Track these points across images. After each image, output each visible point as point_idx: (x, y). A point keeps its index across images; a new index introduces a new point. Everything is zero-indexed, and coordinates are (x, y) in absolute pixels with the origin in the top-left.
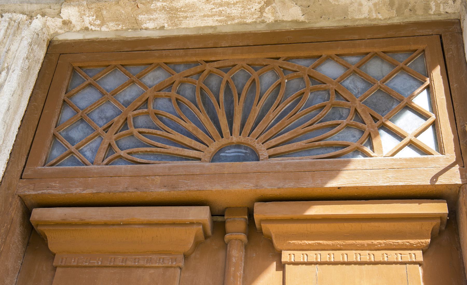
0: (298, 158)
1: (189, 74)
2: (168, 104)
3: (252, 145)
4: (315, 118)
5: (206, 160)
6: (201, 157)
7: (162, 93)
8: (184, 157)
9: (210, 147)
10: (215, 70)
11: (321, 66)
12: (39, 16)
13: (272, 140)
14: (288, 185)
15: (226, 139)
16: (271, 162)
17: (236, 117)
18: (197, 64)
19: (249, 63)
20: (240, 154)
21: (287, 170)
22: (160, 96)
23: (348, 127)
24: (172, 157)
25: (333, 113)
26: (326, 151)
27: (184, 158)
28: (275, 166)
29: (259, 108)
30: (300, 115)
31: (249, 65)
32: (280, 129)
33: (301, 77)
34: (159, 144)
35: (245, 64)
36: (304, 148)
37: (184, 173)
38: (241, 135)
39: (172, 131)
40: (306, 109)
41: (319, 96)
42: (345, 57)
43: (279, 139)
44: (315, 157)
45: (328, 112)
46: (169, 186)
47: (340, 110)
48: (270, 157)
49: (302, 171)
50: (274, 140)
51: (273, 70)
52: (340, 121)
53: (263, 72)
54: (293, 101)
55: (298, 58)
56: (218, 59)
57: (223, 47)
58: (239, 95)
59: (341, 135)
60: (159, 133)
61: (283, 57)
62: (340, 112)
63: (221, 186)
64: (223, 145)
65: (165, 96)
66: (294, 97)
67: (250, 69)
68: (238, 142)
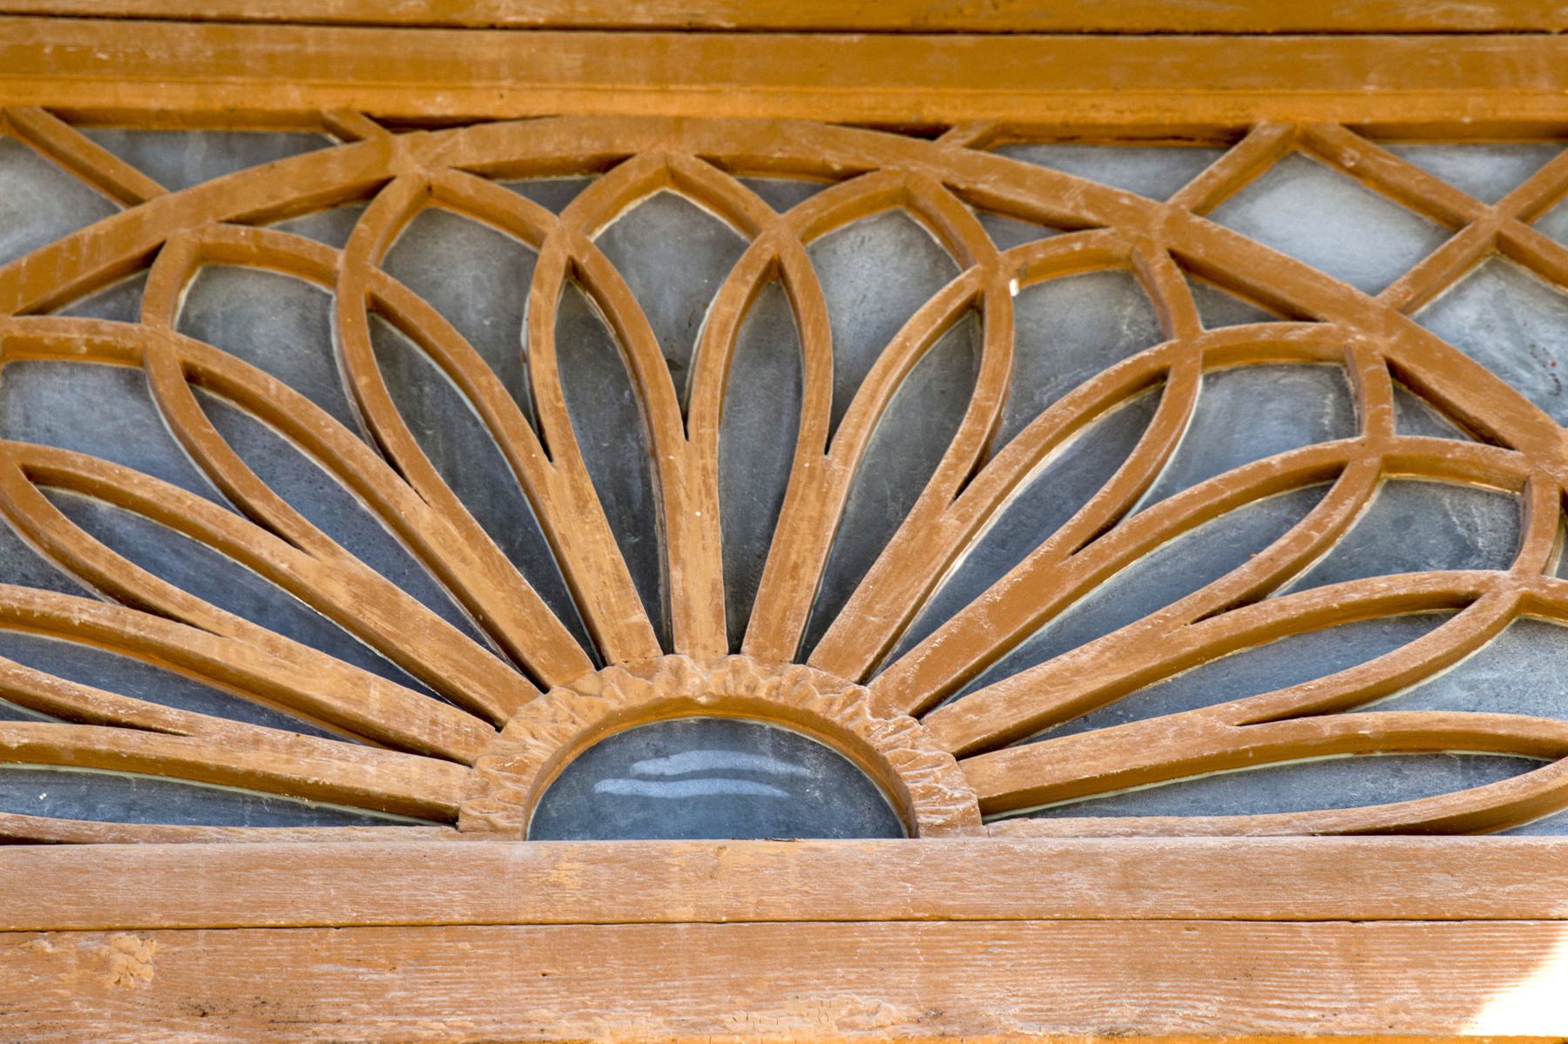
0: (1204, 821)
1: (271, 204)
2: (118, 411)
3: (837, 719)
4: (1284, 551)
5: (499, 819)
6: (453, 798)
7: (69, 327)
8: (306, 802)
9: (512, 725)
10: (467, 185)
11: (1251, 201)
13: (982, 692)
14: (1181, 1012)
15: (632, 671)
16: (1018, 848)
17: (683, 521)
18: (312, 136)
19: (720, 153)
20: (749, 788)
21: (1148, 903)
22: (46, 349)
23: (1527, 622)
24: (209, 797)
25: (1396, 523)
26: (1396, 783)
27: (308, 809)
28: (1055, 877)
29: (846, 462)
30: (1167, 524)
31: (716, 162)
32: (1031, 618)
33: (1118, 268)
34: (101, 700)
35: (686, 160)
36: (1238, 758)
37: (349, 915)
38: (744, 648)
39: (191, 608)
40: (1202, 485)
41: (1272, 405)
42: (1412, 150)
43: (1038, 689)
44: (1333, 818)
45: (1359, 517)
46: (233, 1011)
47: (1447, 501)
48: (991, 809)
49: (1268, 913)
50: (1001, 688)
51: (899, 213)
52: (1466, 579)
53: (833, 220)
54: (1088, 428)
55: (1069, 138)
56: (477, 112)
57: (505, 28)
58: (678, 366)
59: (1486, 675)
60: (85, 617)
61: (965, 125)
62: (1446, 515)
63: (656, 1010)
64: (611, 719)
65: (88, 354)
66: (1096, 401)
67: (734, 191)
68: (725, 702)
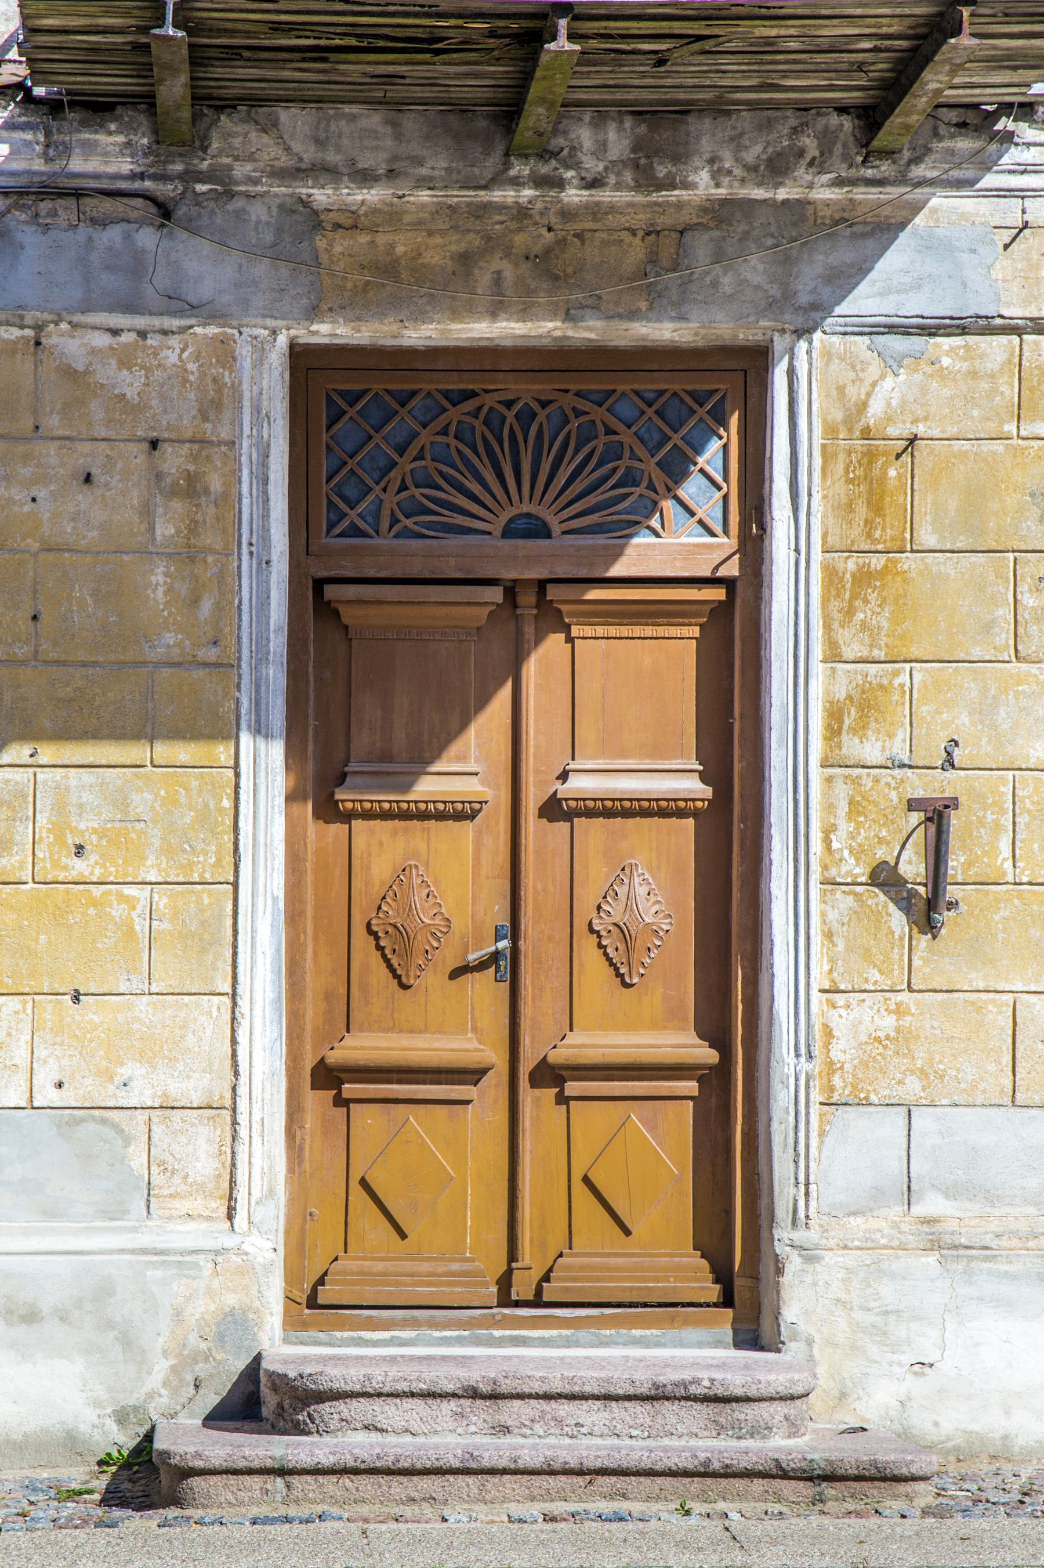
12: (283, 331)
